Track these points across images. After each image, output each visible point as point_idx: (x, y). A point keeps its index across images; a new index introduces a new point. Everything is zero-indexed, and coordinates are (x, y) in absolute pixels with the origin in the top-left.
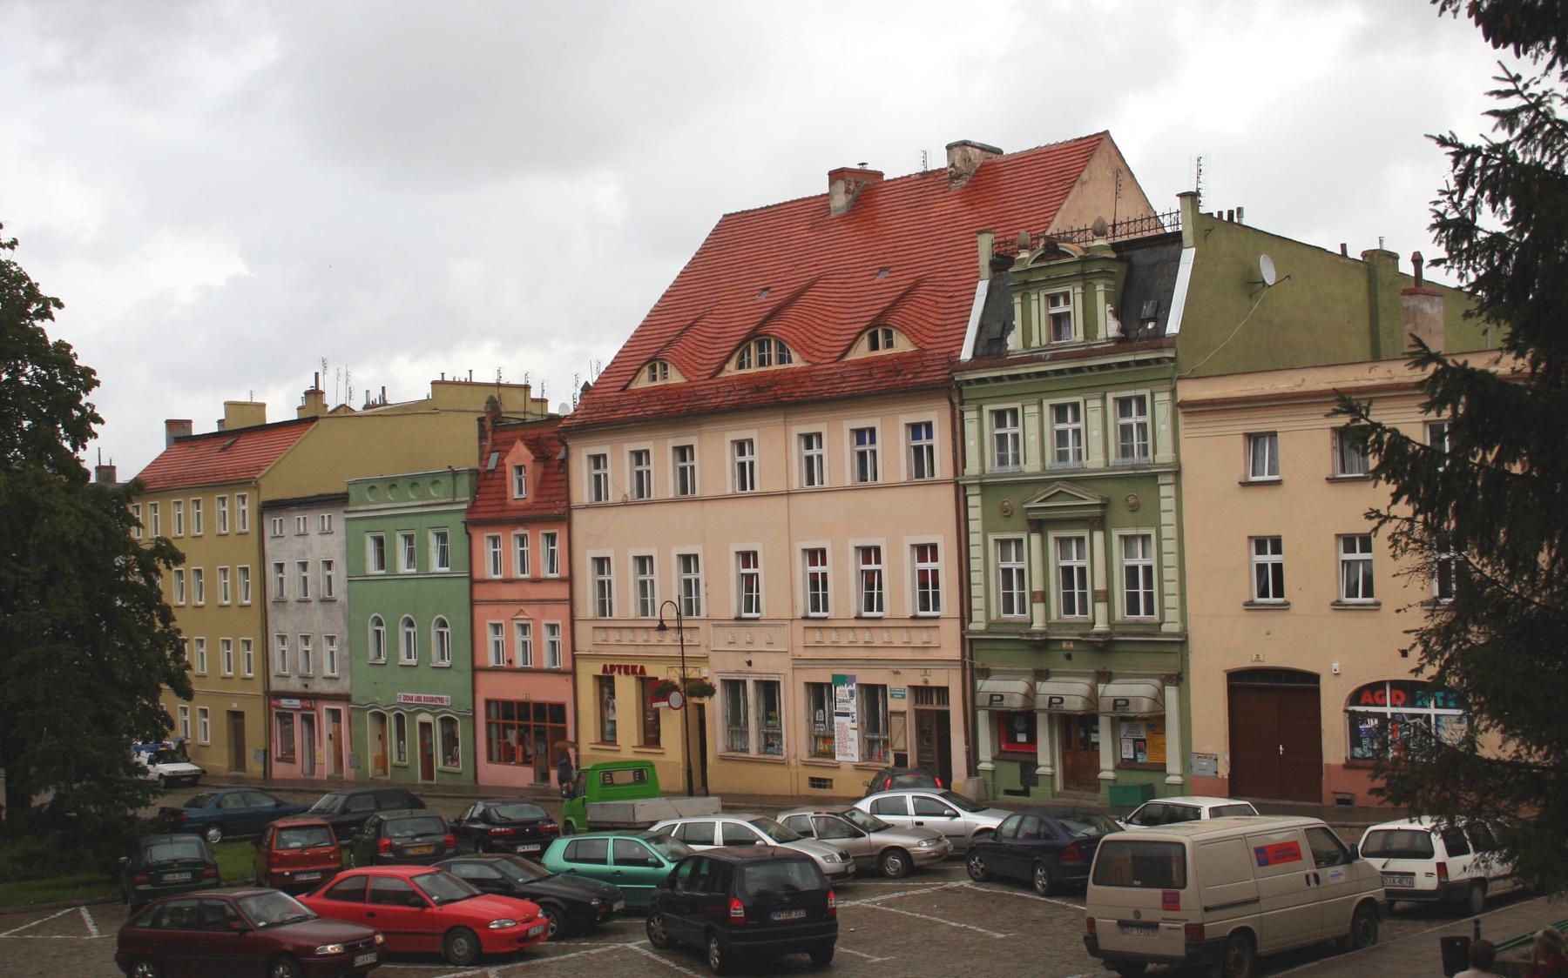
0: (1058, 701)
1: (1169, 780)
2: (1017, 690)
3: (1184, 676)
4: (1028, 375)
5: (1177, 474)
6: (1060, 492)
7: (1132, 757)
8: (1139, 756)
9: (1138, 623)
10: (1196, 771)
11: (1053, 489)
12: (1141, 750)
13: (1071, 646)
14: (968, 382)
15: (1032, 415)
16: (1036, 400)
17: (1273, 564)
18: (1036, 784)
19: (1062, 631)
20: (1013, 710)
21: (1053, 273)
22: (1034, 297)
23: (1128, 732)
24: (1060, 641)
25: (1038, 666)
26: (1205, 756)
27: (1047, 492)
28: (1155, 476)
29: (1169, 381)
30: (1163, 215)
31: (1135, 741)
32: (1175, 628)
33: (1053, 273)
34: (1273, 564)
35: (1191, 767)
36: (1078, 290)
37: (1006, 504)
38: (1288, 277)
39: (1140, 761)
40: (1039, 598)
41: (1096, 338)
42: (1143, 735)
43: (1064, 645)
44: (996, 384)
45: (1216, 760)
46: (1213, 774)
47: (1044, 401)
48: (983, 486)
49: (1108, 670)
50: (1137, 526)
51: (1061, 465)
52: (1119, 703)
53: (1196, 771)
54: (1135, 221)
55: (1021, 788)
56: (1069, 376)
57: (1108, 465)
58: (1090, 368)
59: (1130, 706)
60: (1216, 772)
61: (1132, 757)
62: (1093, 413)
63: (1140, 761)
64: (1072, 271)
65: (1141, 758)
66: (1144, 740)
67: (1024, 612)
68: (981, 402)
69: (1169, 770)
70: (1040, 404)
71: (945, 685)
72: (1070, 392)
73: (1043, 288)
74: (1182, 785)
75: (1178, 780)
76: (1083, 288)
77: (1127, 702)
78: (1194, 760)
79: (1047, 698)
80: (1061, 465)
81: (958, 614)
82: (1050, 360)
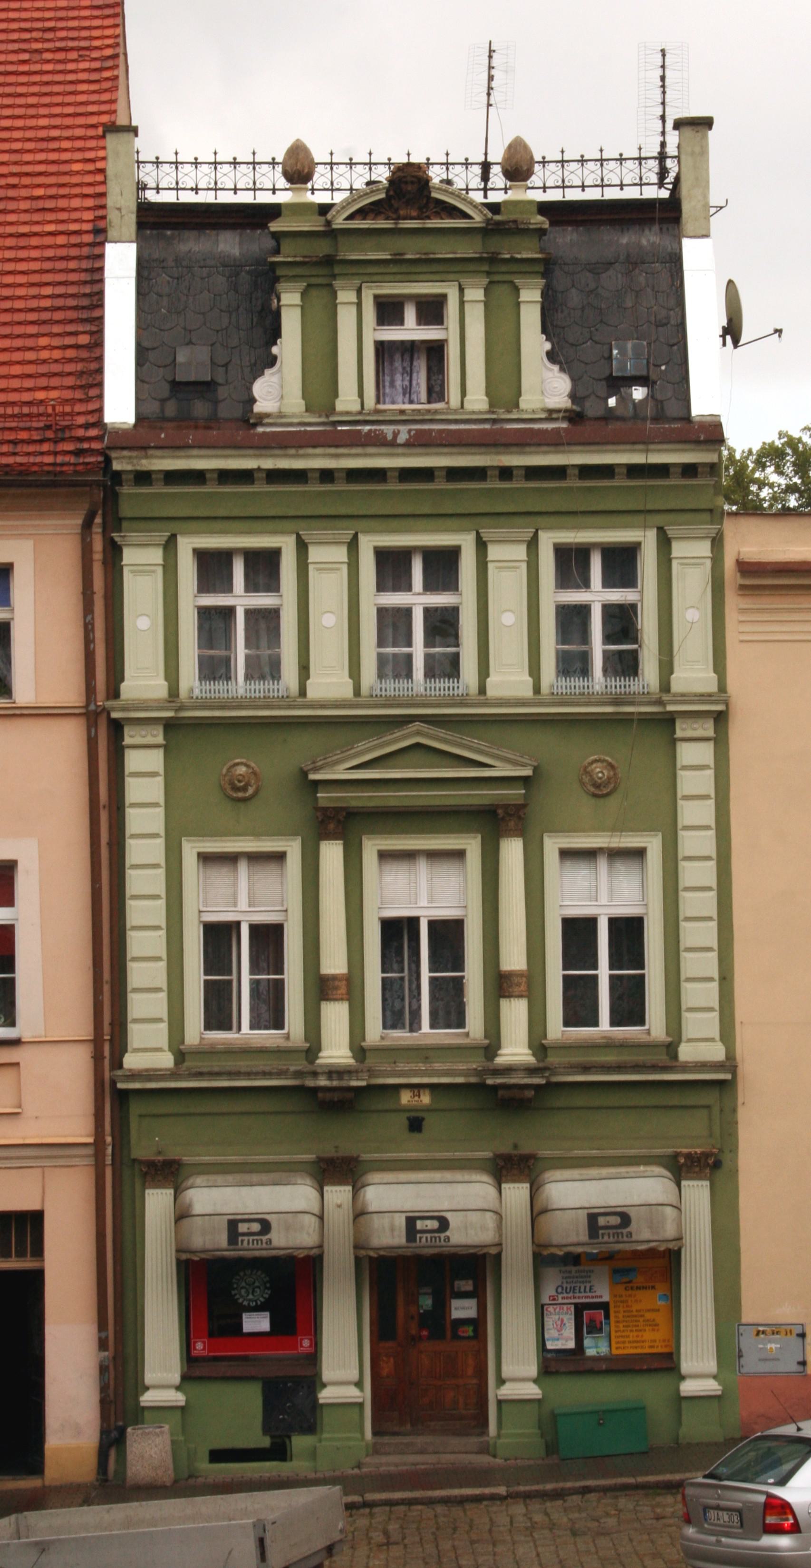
0: (434, 1224)
1: (688, 1387)
2: (301, 1206)
3: (726, 1158)
4: (327, 475)
5: (721, 719)
6: (418, 745)
7: (571, 1345)
8: (587, 1342)
9: (230, 1052)
10: (751, 1364)
11: (404, 737)
12: (595, 1329)
13: (426, 1099)
14: (143, 477)
15: (327, 567)
16: (528, 533)
17: (432, 924)
18: (311, 1428)
19: (401, 1066)
20: (302, 1254)
21: (412, 249)
22: (346, 296)
23: (560, 1289)
24: (397, 1088)
25: (329, 1151)
26: (776, 1330)
27: (381, 746)
28: (668, 721)
29: (706, 516)
30: (544, 162)
31: (579, 1309)
32: (716, 1052)
33: (412, 249)
34: (432, 924)
35: (740, 1356)
36: (475, 294)
37: (242, 770)
38: (779, 331)
39: (590, 1352)
40: (343, 990)
41: (517, 406)
42: (603, 1292)
43: (406, 1098)
44: (451, 486)
45: (802, 1335)
46: (795, 1368)
47: (180, 539)
48: (170, 726)
49: (525, 1150)
50: (616, 828)
51: (393, 687)
52: (602, 1221)
53: (751, 1364)
54: (621, 160)
55: (265, 1442)
56: (393, 486)
57: (357, 692)
58: (506, 473)
59: (633, 1227)
60: (803, 1363)
61: (571, 1345)
62: (505, 574)
63: (590, 1352)
64: (467, 249)
65: (594, 1347)
66: (605, 1306)
67: (278, 1023)
68: (174, 527)
69: (686, 1366)
70: (170, 546)
71: (36, 1206)
72: (271, 525)
73: (372, 278)
74: (182, 1408)
75: (711, 1386)
76: (487, 291)
77: (625, 1219)
78: (747, 1341)
79: (400, 1221)
80: (393, 687)
81: (86, 1031)
82: (408, 444)
